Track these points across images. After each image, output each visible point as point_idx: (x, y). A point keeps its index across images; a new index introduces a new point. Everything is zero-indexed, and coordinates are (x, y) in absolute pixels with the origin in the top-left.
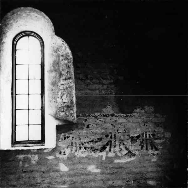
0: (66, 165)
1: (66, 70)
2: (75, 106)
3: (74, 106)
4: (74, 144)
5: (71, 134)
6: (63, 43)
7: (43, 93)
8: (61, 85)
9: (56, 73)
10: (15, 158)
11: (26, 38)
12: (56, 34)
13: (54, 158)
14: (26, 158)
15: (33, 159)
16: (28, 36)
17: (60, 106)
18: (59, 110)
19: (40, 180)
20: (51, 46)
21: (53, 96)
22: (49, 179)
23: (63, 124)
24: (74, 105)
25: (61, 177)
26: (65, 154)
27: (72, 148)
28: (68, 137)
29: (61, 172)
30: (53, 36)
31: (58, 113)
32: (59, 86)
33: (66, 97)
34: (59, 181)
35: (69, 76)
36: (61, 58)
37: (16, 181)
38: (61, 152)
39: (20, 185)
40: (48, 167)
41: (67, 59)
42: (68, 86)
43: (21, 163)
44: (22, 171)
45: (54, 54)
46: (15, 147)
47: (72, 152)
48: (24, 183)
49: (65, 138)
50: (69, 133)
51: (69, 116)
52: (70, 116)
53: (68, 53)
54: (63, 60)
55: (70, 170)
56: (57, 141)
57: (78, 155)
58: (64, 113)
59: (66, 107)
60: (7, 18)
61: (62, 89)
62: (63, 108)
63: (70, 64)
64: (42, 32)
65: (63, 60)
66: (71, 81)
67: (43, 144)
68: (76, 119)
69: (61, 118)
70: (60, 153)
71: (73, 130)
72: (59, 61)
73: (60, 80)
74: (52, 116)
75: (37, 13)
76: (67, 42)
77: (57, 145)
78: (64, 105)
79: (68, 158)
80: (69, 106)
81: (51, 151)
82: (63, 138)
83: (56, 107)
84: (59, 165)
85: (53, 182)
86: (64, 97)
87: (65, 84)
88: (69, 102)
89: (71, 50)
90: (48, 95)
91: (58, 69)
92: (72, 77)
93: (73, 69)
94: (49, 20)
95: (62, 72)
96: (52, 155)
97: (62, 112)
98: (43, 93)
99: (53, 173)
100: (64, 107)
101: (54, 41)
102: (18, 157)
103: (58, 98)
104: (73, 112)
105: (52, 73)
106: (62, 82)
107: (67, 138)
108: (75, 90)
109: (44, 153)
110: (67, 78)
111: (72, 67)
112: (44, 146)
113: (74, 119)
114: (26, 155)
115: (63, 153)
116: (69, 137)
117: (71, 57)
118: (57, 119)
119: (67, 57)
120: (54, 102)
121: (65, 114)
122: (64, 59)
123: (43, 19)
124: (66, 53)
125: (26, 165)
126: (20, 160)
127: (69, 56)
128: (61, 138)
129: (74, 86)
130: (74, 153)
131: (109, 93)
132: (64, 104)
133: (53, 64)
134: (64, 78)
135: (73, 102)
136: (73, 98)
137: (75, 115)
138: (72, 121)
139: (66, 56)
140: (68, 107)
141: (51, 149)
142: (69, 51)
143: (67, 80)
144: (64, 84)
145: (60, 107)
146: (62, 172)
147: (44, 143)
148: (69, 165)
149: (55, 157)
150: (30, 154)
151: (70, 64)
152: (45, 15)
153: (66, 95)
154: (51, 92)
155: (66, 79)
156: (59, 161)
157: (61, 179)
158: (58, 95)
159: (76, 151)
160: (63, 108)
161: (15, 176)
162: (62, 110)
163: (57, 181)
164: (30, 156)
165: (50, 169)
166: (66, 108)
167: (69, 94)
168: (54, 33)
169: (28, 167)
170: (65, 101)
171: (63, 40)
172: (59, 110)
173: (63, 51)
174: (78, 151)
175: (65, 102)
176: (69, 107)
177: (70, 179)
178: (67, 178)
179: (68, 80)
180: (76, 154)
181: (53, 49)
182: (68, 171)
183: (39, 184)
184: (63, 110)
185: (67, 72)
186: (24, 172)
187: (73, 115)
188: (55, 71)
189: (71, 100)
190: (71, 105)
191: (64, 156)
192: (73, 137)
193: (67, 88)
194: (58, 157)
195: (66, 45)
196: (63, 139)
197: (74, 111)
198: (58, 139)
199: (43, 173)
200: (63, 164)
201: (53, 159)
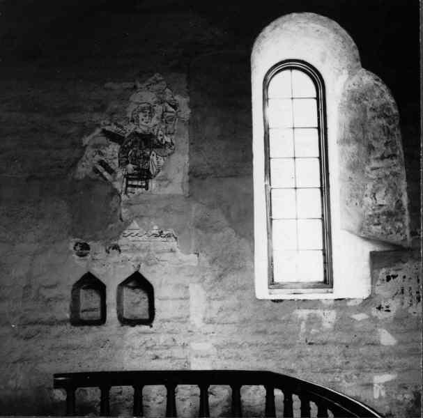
0: (392, 332)
1: (382, 139)
2: (407, 212)
3: (404, 214)
4: (406, 290)
5: (400, 269)
6: (376, 82)
7: (325, 189)
8: (372, 169)
9: (359, 147)
10: (290, 316)
11: (287, 72)
12: (363, 66)
13: (367, 317)
14: (312, 316)
15: (325, 319)
16: (291, 68)
17: (370, 213)
18: (367, 222)
19: (341, 361)
20: (348, 91)
21: (354, 192)
22: (359, 360)
23: (386, 249)
24: (405, 210)
25: (382, 358)
26: (389, 311)
27: (403, 298)
28: (394, 277)
29: (381, 347)
30: (357, 70)
31: (366, 227)
32: (368, 173)
33: (386, 195)
34: (377, 364)
35: (390, 151)
36: (370, 115)
37: (294, 362)
38: (381, 306)
39: (303, 369)
40: (355, 336)
41: (386, 116)
42: (388, 173)
43: (303, 325)
44: (306, 341)
45: (354, 105)
46: (276, 294)
47: (404, 307)
48: (309, 365)
49: (388, 279)
50: (395, 268)
51: (391, 233)
52: (394, 233)
53: (388, 104)
54: (376, 118)
55: (400, 342)
56: (372, 284)
57: (415, 313)
58: (380, 227)
59: (385, 215)
60: (264, 37)
61: (375, 177)
62: (379, 217)
63: (391, 127)
64: (323, 61)
65: (376, 118)
66: (395, 161)
67: (330, 290)
68: (409, 239)
69: (373, 237)
70: (379, 308)
71: (404, 263)
72: (365, 121)
73: (369, 160)
74: (351, 232)
75: (322, 23)
76: (385, 81)
77: (373, 289)
78: (380, 211)
79: (395, 318)
80: (391, 212)
81: (362, 303)
82: (385, 279)
83: (361, 215)
84: (377, 332)
85: (367, 366)
86: (379, 196)
87: (382, 168)
88: (392, 205)
89: (396, 99)
90: (341, 190)
91: (364, 137)
92: (398, 153)
93: (400, 137)
94: (349, 37)
95: (375, 144)
96: (364, 312)
97: (375, 225)
98: (325, 189)
99: (367, 347)
100: (379, 214)
101: (355, 79)
102: (297, 315)
103: (366, 196)
104: (401, 225)
105: (349, 146)
106: (374, 164)
107: (392, 278)
108: (407, 180)
109: (347, 307)
110: (385, 156)
111: (398, 132)
112: (332, 292)
113: (405, 240)
114: (312, 311)
115: (386, 309)
116: (397, 276)
117: (395, 111)
118: (367, 239)
119: (385, 111)
120: (356, 204)
121: (384, 228)
122: (378, 117)
123: (332, 35)
124: (383, 103)
125: (313, 330)
126: (302, 320)
127: (389, 110)
128: (380, 278)
129: (403, 173)
130: (408, 308)
131: (144, 184)
132: (379, 209)
133: (350, 126)
134: (378, 155)
135: (401, 205)
136: (401, 195)
137: (408, 232)
138: (400, 243)
139: (383, 111)
140: (389, 214)
141: (360, 299)
142: (388, 98)
143: (385, 160)
144: (378, 168)
145: (370, 216)
146: (383, 346)
147: (332, 287)
148: (397, 333)
149: (370, 315)
150: (321, 309)
151: (391, 127)
152: (338, 27)
153: (384, 190)
154: (348, 183)
155: (382, 158)
156: (378, 325)
157: (382, 361)
158: (364, 190)
159: (411, 305)
160: (379, 217)
161: (292, 351)
162: (376, 221)
163: (373, 363)
164: (319, 312)
165: (360, 340)
166: (384, 217)
167: (391, 188)
168: (359, 63)
169: (316, 334)
170: (382, 203)
171: (377, 77)
172: (367, 222)
173: (375, 100)
174: (414, 305)
175: (381, 206)
176: (394, 216)
177: (400, 361)
178: (395, 359)
179: (390, 161)
180: (411, 310)
181: (352, 96)
182: (395, 346)
183: (338, 370)
184: (378, 221)
185: (386, 144)
186: (310, 344)
187: (402, 231)
188: (358, 140)
189: (398, 201)
190: (397, 211)
191: (387, 315)
192: (404, 277)
193: (386, 177)
194: (376, 317)
195: (384, 88)
196: (383, 280)
197: (403, 223)
198: (374, 278)
199: (347, 347)
200: (384, 331)
201: (366, 319)
